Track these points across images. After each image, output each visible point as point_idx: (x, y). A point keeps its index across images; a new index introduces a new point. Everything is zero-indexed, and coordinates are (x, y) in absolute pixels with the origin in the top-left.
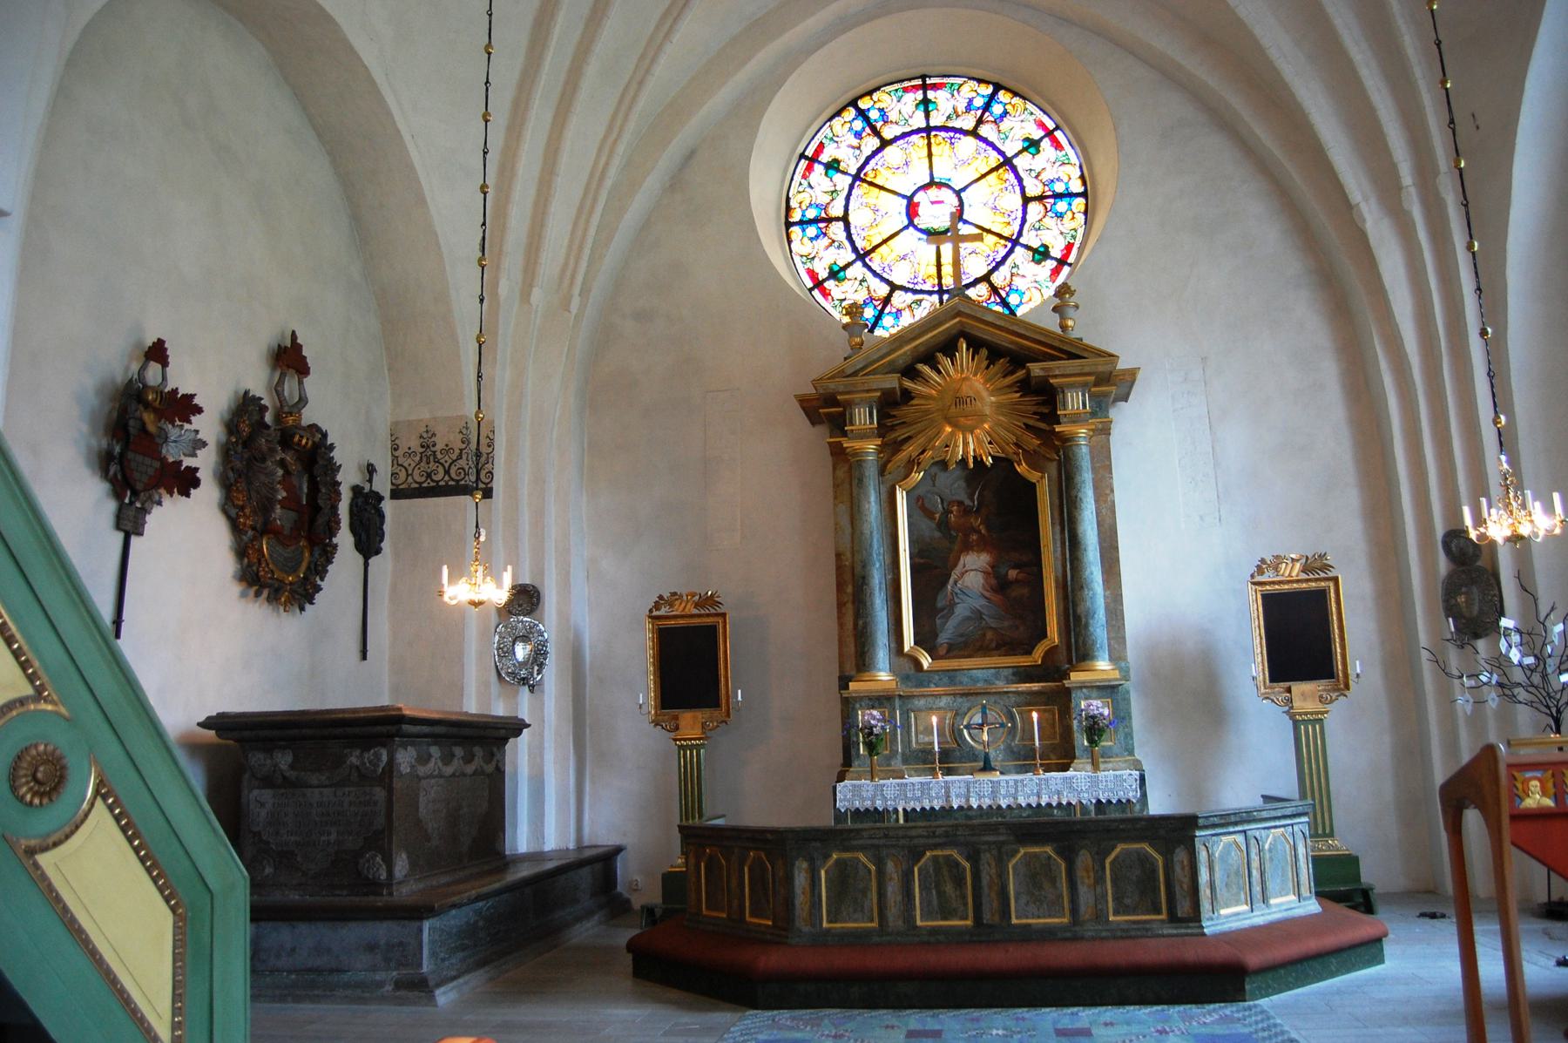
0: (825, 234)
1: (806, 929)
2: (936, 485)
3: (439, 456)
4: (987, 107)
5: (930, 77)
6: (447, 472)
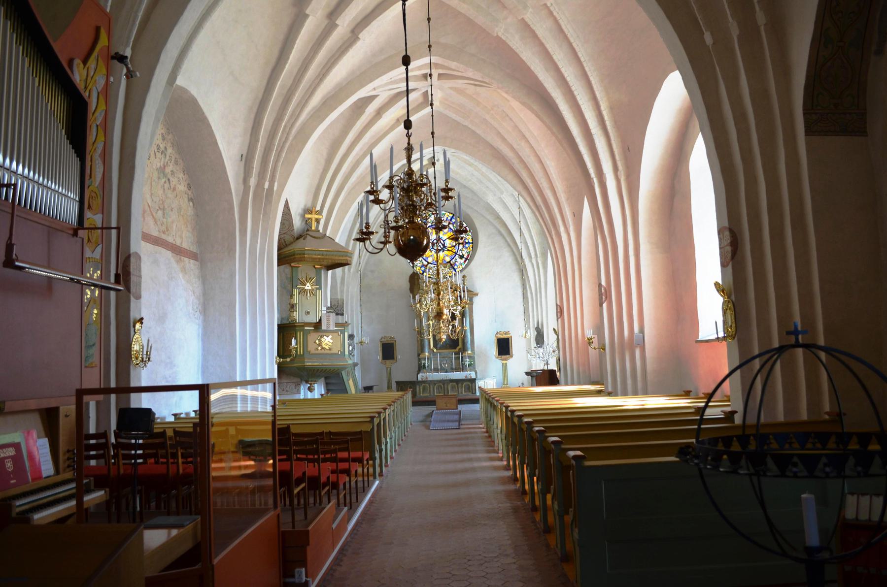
4: (451, 220)
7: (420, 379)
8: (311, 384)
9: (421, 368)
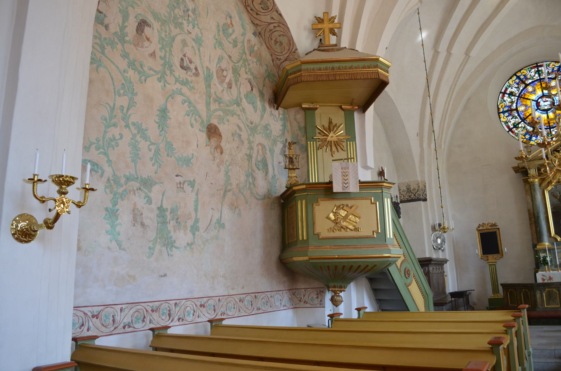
0: (511, 115)
1: (541, 307)
2: (557, 188)
3: (412, 191)
5: (539, 63)
6: (415, 195)
7: (539, 281)
8: (335, 292)
9: (539, 264)
